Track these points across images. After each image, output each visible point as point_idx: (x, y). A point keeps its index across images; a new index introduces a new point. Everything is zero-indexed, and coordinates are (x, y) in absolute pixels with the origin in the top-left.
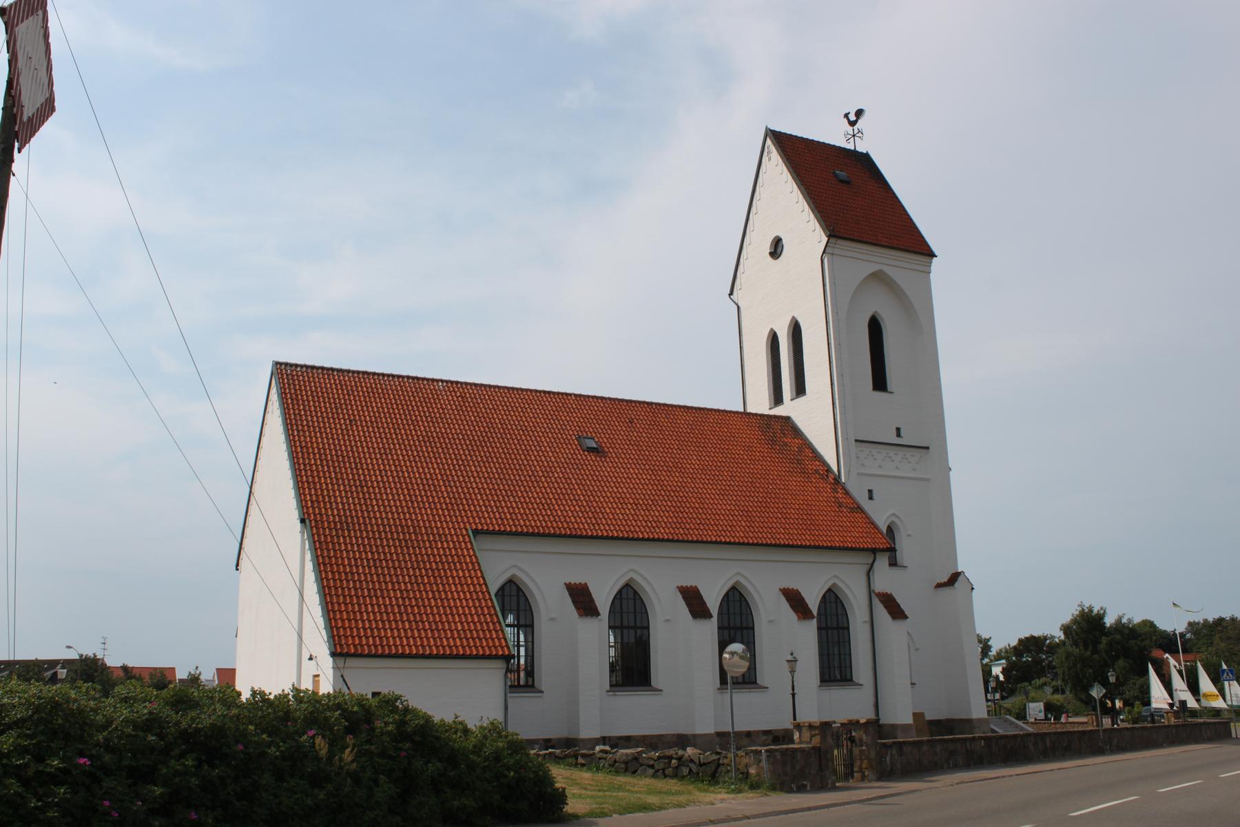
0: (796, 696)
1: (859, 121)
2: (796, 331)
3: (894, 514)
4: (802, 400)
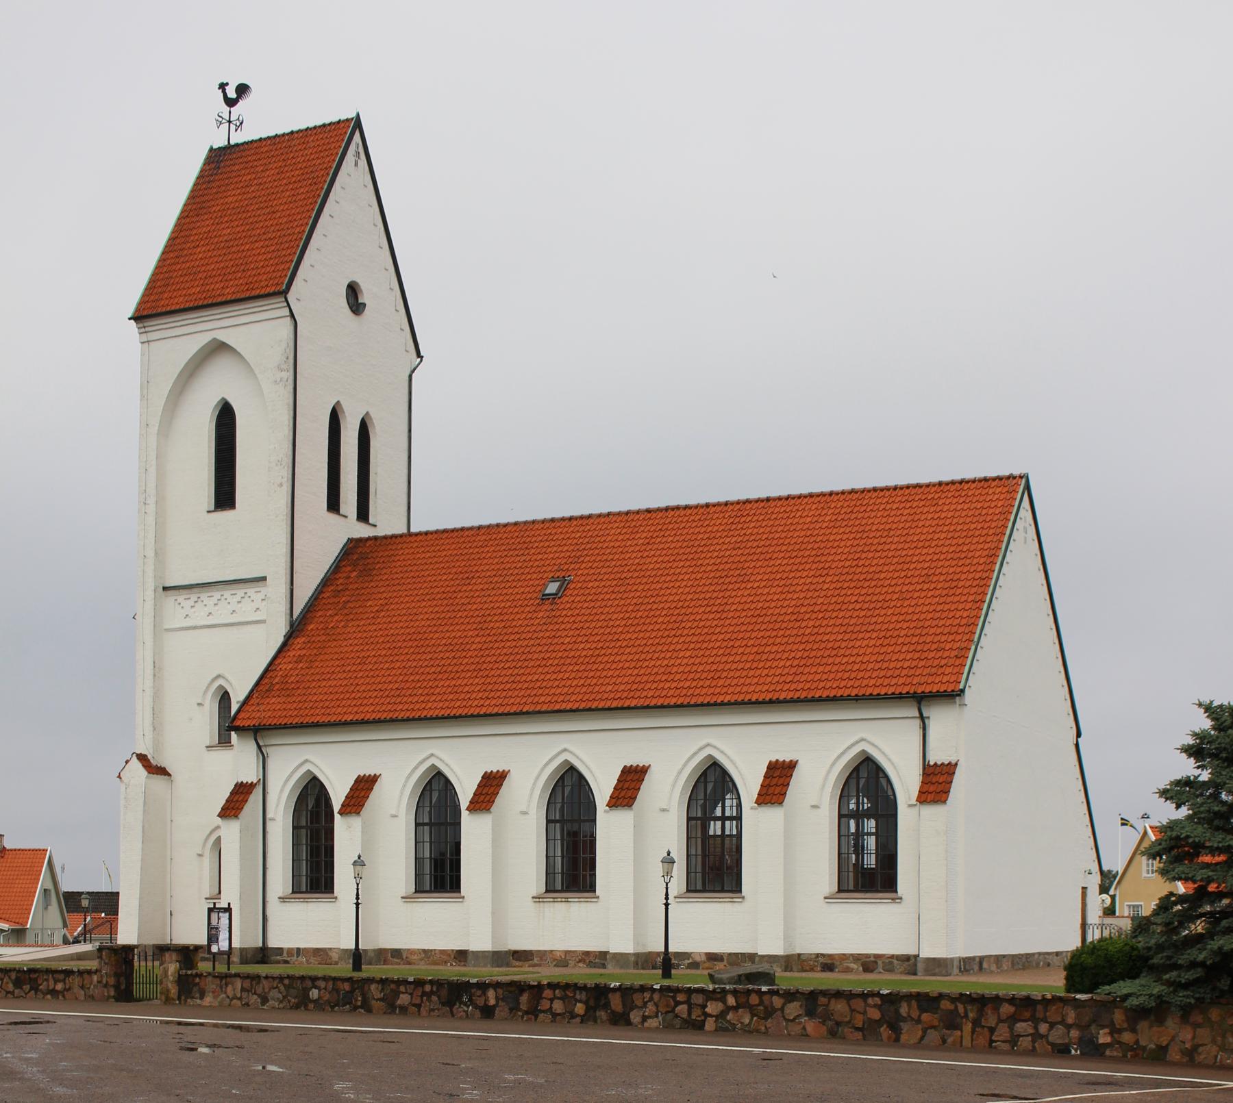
0: (669, 907)
1: (241, 103)
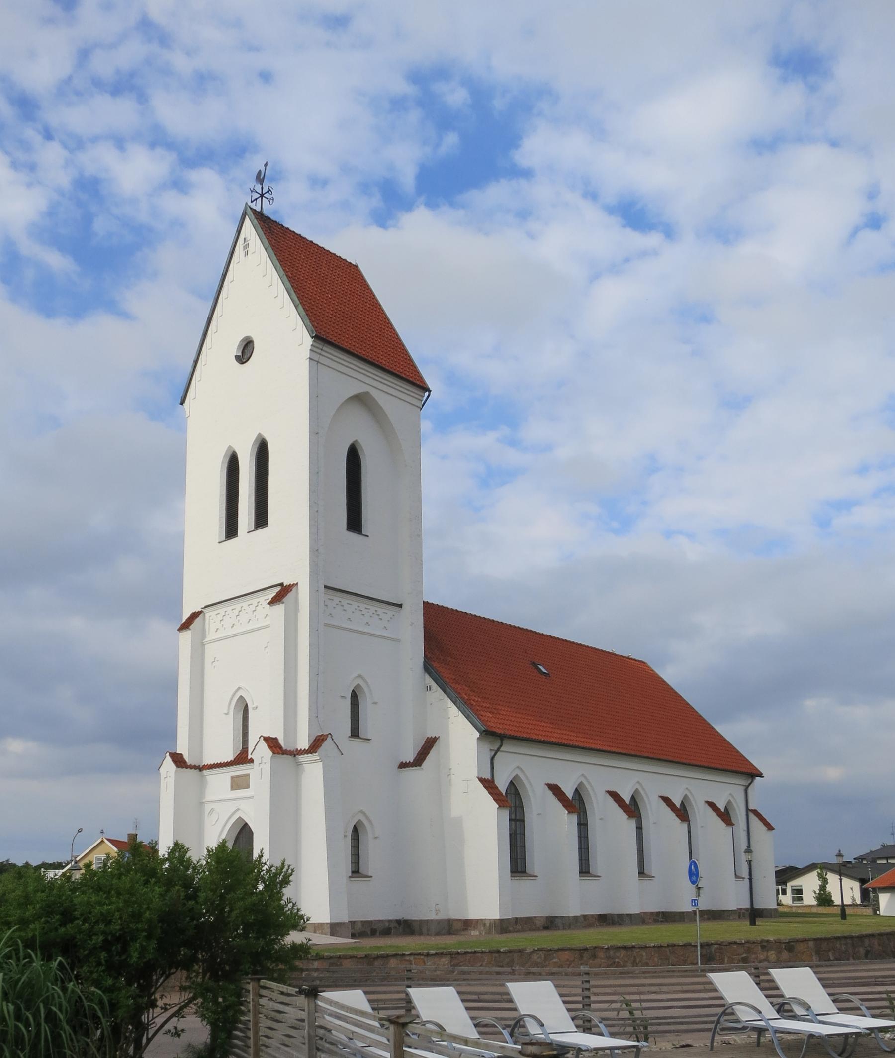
2: (262, 452)
3: (360, 676)
4: (262, 532)
